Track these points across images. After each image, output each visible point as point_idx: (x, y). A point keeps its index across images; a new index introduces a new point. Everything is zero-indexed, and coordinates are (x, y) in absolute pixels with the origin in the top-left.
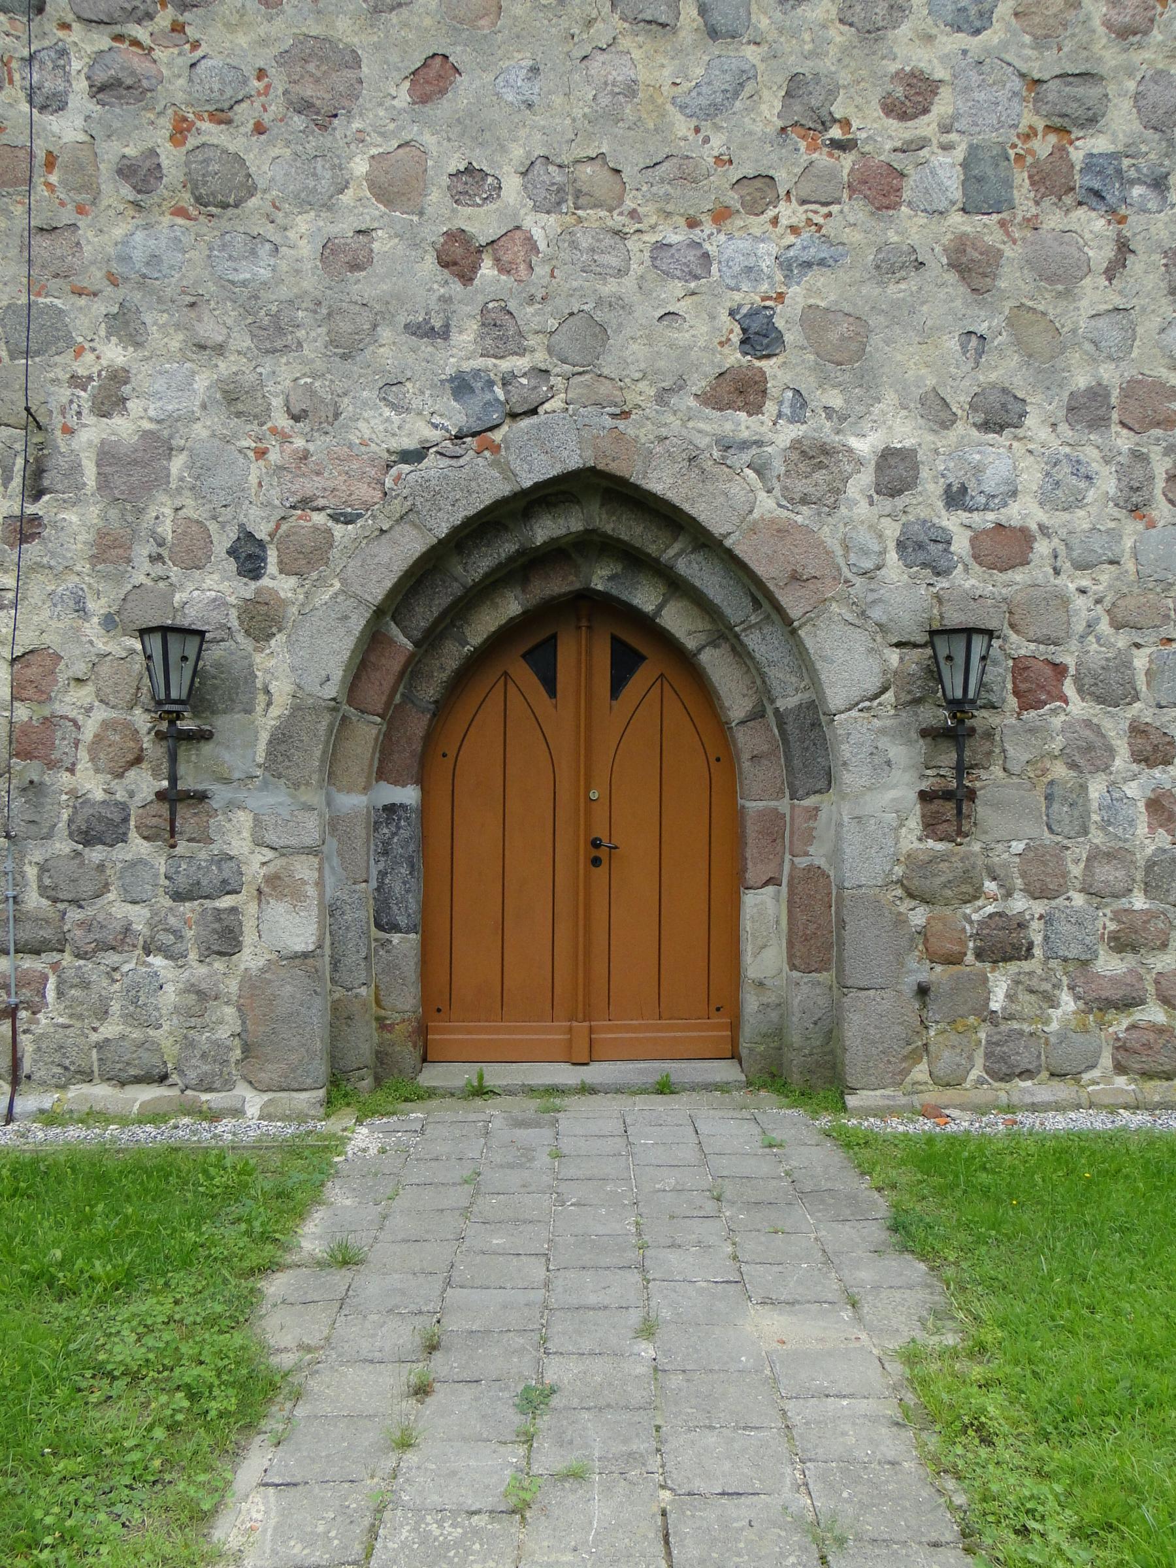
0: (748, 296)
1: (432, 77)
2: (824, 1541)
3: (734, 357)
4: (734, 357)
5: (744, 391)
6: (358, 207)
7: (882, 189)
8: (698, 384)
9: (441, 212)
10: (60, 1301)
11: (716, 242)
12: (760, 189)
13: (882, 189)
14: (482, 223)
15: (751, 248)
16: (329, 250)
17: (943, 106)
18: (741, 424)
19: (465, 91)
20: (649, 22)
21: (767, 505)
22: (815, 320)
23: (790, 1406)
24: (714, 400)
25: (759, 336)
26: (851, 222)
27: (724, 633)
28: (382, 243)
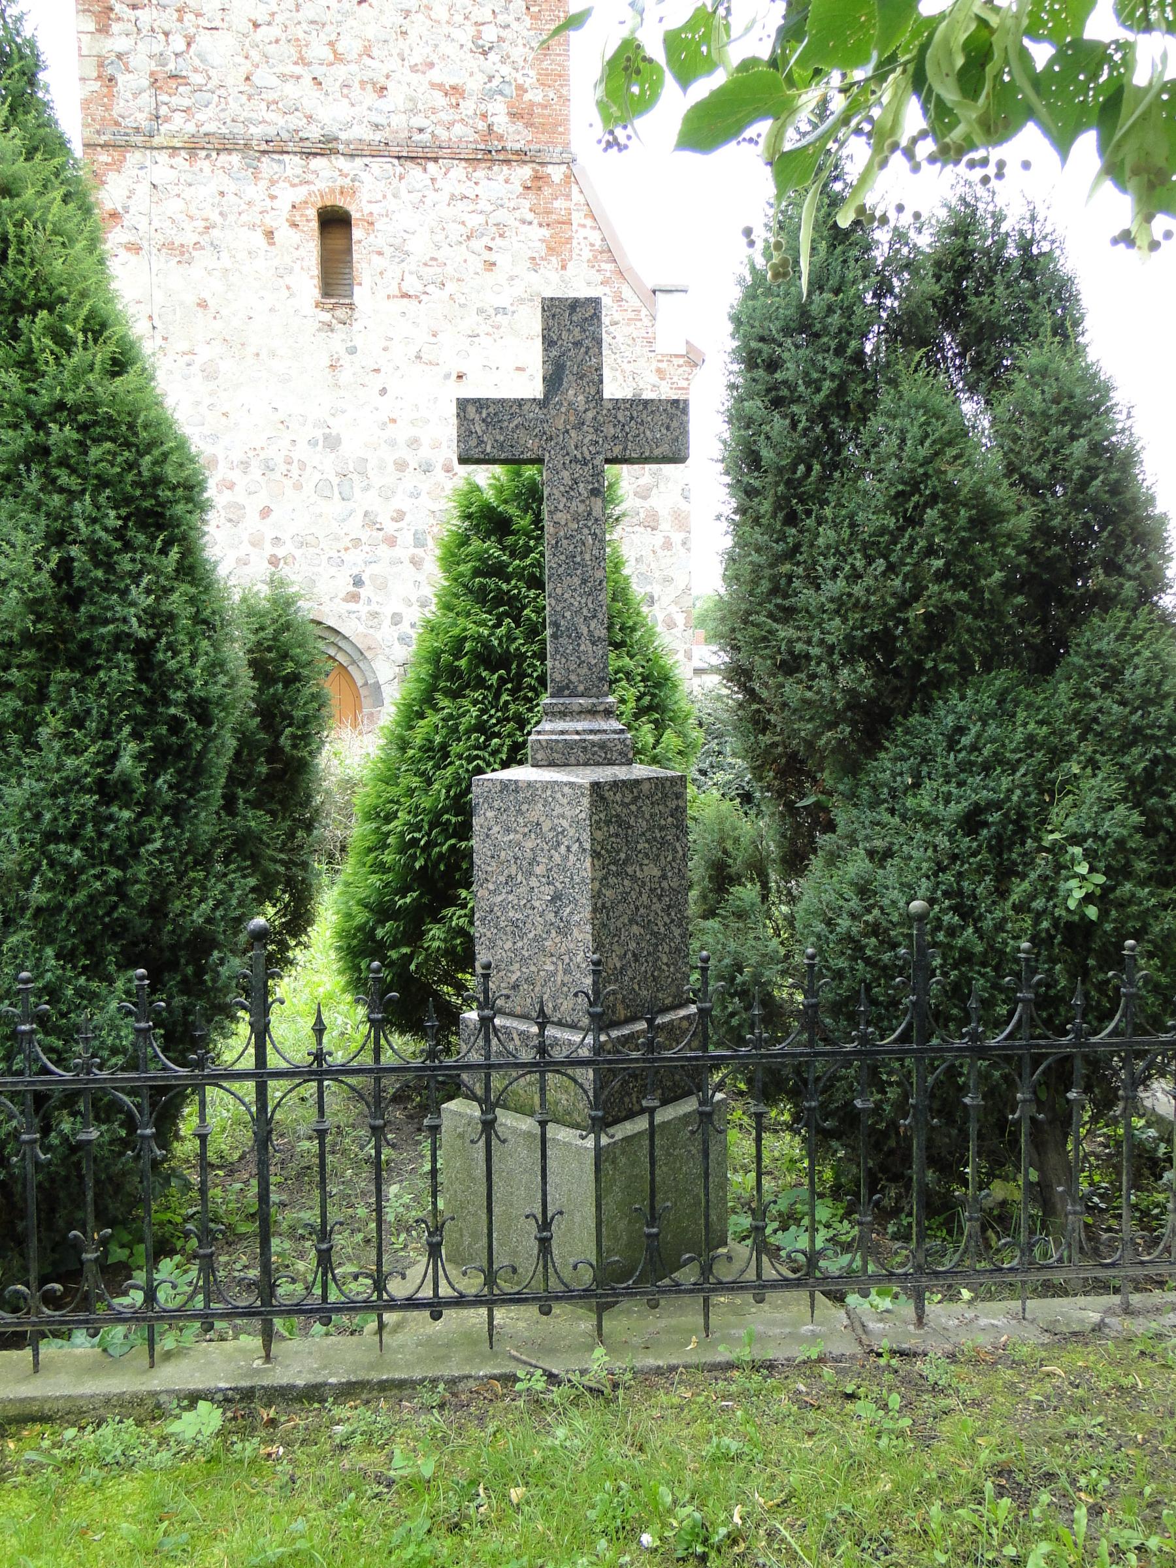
0: (355, 572)
1: (266, 512)
2: (5, 190)
3: (351, 588)
4: (351, 588)
5: (354, 597)
6: (246, 548)
7: (391, 542)
8: (342, 595)
9: (269, 550)
10: (1003, 1204)
11: (345, 556)
12: (357, 542)
13: (391, 542)
14: (280, 552)
15: (355, 558)
16: (238, 560)
17: (408, 518)
18: (352, 606)
19: (273, 516)
20: (274, 148)
21: (361, 629)
22: (373, 577)
23: (397, 1288)
24: (345, 600)
25: (358, 582)
26: (384, 551)
27: (354, 662)
28: (252, 558)
